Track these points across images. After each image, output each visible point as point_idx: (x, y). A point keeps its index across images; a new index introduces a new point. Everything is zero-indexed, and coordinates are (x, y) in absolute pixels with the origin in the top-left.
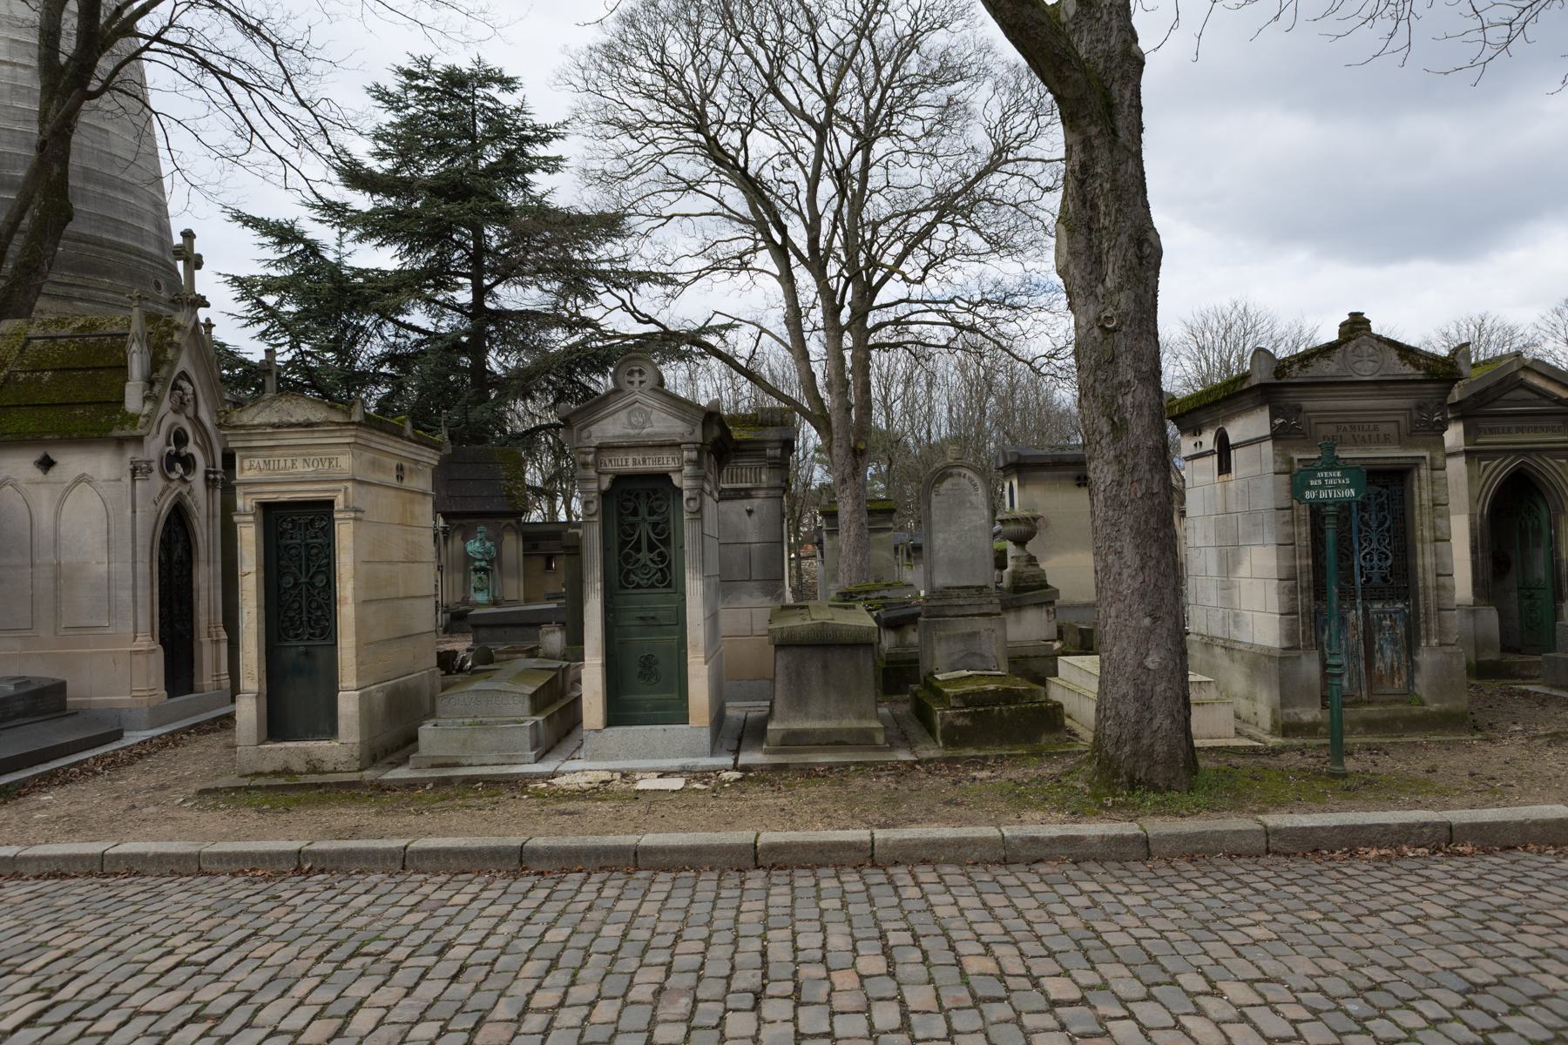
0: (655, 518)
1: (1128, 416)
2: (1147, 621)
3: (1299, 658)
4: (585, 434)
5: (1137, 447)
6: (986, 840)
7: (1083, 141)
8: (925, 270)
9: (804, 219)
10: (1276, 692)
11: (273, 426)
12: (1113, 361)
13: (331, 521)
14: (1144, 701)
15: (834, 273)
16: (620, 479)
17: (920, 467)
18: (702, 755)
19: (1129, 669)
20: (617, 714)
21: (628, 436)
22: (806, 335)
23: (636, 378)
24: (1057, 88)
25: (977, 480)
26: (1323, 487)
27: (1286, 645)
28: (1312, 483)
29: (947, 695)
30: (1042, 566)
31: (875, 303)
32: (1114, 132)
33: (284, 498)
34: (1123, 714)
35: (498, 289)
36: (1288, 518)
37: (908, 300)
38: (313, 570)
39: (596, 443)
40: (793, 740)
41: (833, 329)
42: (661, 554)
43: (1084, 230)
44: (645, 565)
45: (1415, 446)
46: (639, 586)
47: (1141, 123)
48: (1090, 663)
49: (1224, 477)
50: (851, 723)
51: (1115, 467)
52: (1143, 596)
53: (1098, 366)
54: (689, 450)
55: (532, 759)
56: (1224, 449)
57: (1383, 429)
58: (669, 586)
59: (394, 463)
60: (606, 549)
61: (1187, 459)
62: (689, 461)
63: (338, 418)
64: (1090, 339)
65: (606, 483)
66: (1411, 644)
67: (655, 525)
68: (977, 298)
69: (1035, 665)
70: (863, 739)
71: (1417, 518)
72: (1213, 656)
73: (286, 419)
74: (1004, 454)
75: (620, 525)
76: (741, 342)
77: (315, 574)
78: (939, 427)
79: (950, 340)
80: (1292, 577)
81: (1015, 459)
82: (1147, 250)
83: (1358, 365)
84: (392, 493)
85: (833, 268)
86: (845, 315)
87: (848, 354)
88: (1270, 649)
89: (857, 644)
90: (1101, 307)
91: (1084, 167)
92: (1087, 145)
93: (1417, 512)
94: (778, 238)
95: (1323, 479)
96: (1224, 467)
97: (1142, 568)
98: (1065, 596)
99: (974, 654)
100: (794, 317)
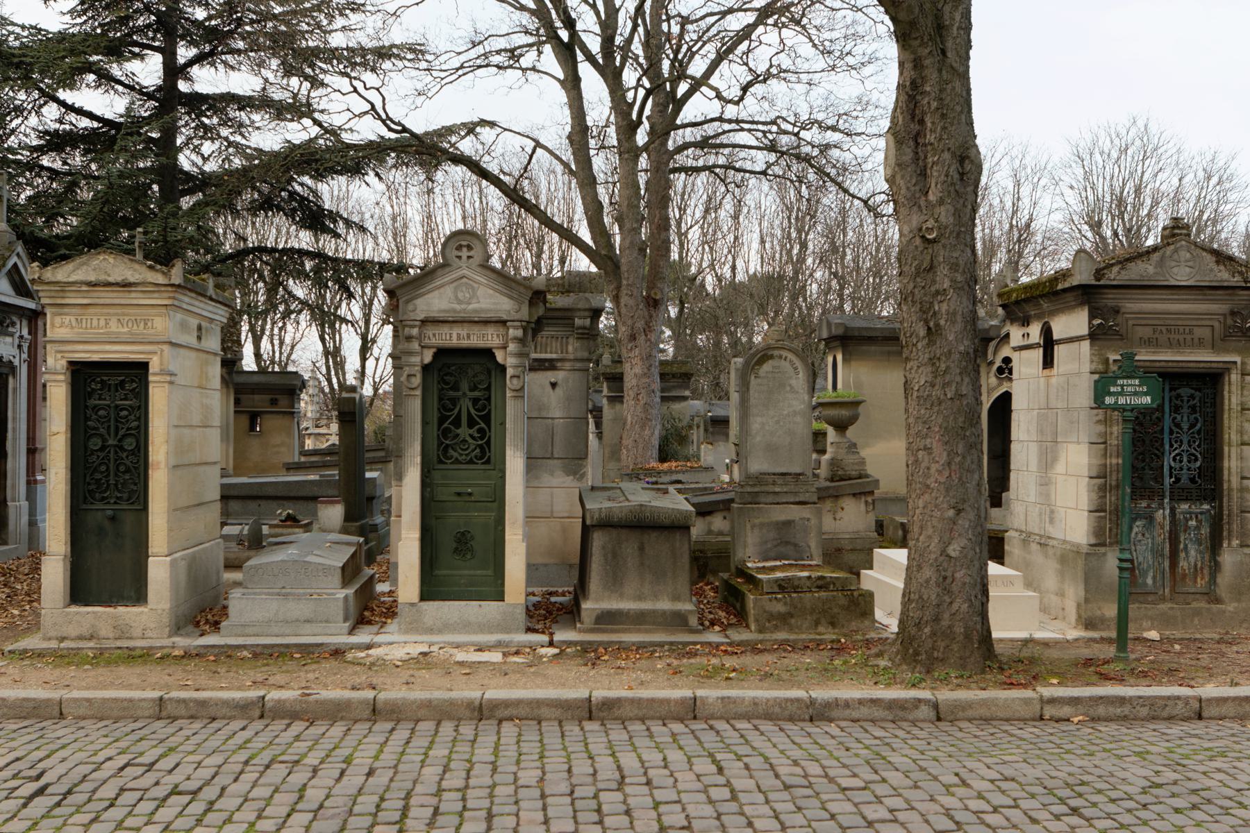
0: (476, 394)
1: (942, 322)
2: (951, 513)
3: (1104, 554)
4: (410, 307)
5: (950, 352)
6: (798, 700)
7: (915, 60)
8: (745, 89)
9: (597, 13)
10: (1081, 587)
11: (90, 284)
12: (931, 268)
13: (146, 384)
14: (945, 582)
15: (633, 83)
16: (442, 353)
17: (721, 313)
18: (517, 631)
19: (933, 556)
20: (434, 587)
21: (455, 311)
22: (592, 152)
23: (464, 253)
24: (891, 10)
25: (798, 363)
26: (1122, 393)
27: (1093, 541)
28: (1112, 389)
29: (760, 580)
30: (865, 453)
31: (678, 122)
32: (944, 52)
33: (96, 358)
34: (925, 597)
35: (195, 71)
36: (1101, 417)
37: (720, 119)
38: (121, 433)
39: (422, 317)
40: (607, 619)
41: (628, 151)
42: (481, 431)
43: (912, 143)
44: (465, 441)
45: (1227, 351)
46: (457, 461)
47: (970, 41)
48: (900, 556)
49: (1047, 372)
50: (665, 605)
51: (929, 369)
52: (947, 490)
53: (918, 274)
54: (515, 328)
55: (346, 630)
56: (1049, 344)
57: (1198, 332)
58: (488, 462)
59: (194, 322)
60: (425, 423)
61: (1016, 349)
62: (515, 338)
63: (160, 279)
64: (911, 248)
65: (428, 357)
66: (1215, 544)
67: (475, 401)
68: (804, 117)
69: (849, 558)
70: (677, 621)
71: (1226, 422)
72: (1030, 553)
73: (103, 278)
74: (829, 324)
75: (440, 399)
76: (504, 153)
77: (124, 436)
78: (747, 263)
79: (769, 165)
80: (1102, 475)
81: (840, 331)
82: (968, 166)
83: (1175, 270)
84: (193, 354)
85: (630, 76)
86: (641, 137)
87: (642, 179)
88: (1078, 545)
89: (676, 527)
90: (924, 218)
91: (914, 84)
92: (917, 64)
93: (1226, 416)
94: (564, 35)
95: (1122, 386)
96: (1048, 362)
97: (949, 464)
98: (883, 489)
99: (787, 543)
100: (580, 133)
